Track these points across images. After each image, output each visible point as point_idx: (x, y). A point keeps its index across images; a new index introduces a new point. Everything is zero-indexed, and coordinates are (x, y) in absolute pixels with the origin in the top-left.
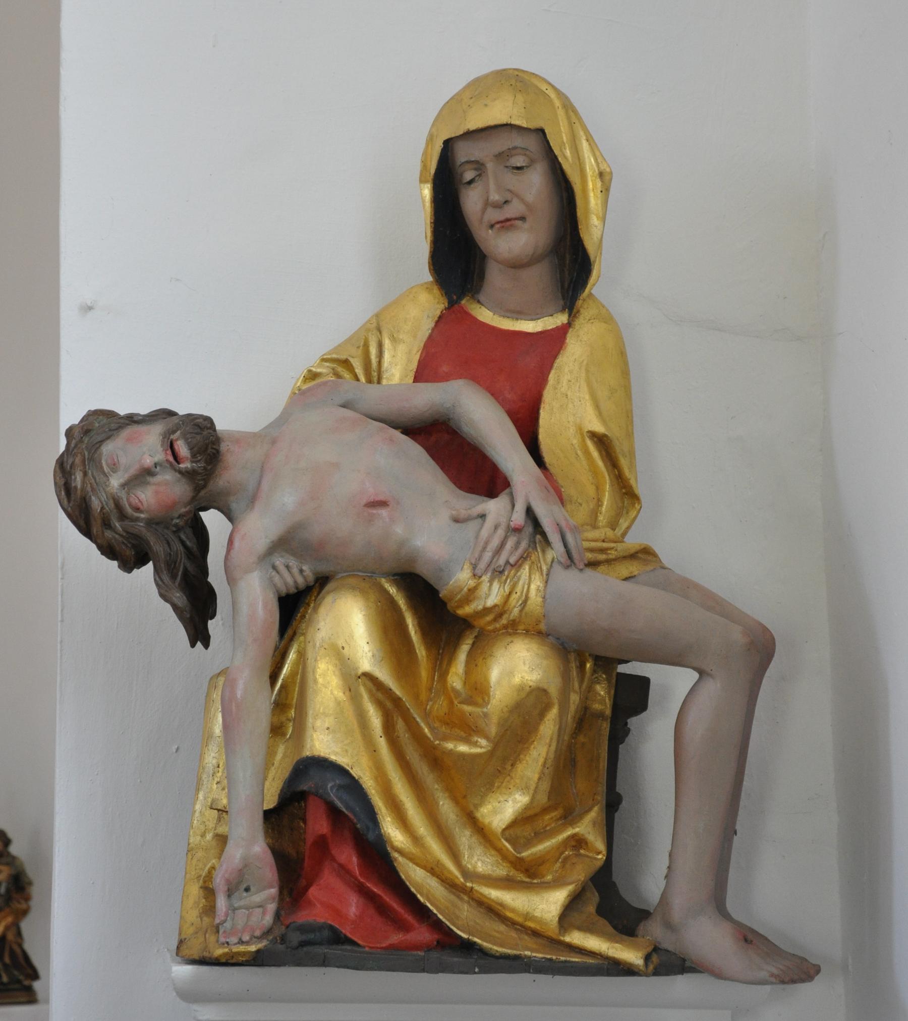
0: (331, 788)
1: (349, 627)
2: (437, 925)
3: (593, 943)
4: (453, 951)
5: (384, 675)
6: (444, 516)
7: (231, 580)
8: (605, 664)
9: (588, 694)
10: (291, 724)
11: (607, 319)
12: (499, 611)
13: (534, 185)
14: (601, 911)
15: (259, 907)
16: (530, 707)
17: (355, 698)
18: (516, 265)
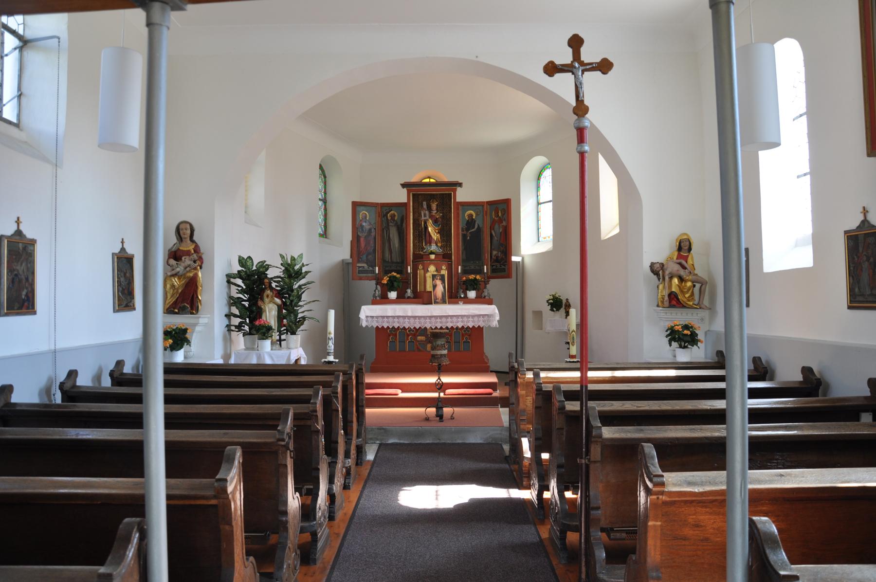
4: (684, 307)
10: (543, 374)
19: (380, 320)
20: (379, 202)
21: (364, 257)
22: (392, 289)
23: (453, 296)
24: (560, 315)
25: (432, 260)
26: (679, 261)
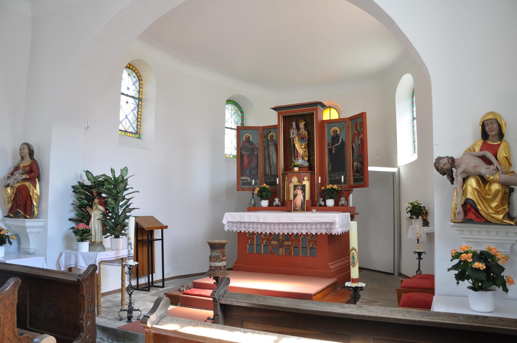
0: (470, 202)
1: (472, 182)
2: (485, 219)
3: (507, 221)
4: (487, 222)
5: (477, 188)
6: (485, 168)
7: (457, 177)
8: (508, 186)
9: (505, 190)
11: (506, 142)
12: (493, 180)
13: (495, 126)
14: (508, 217)
15: (461, 216)
16: (497, 192)
17: (473, 191)
18: (493, 136)
19: (239, 225)
20: (261, 126)
21: (248, 172)
22: (262, 198)
23: (313, 204)
24: (418, 223)
25: (295, 172)
26: (482, 153)
